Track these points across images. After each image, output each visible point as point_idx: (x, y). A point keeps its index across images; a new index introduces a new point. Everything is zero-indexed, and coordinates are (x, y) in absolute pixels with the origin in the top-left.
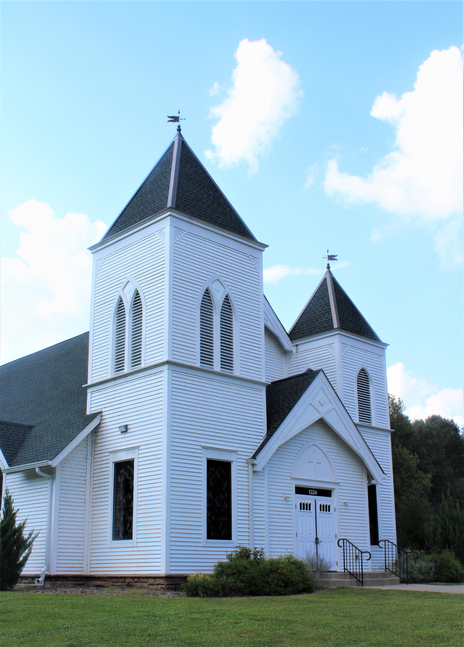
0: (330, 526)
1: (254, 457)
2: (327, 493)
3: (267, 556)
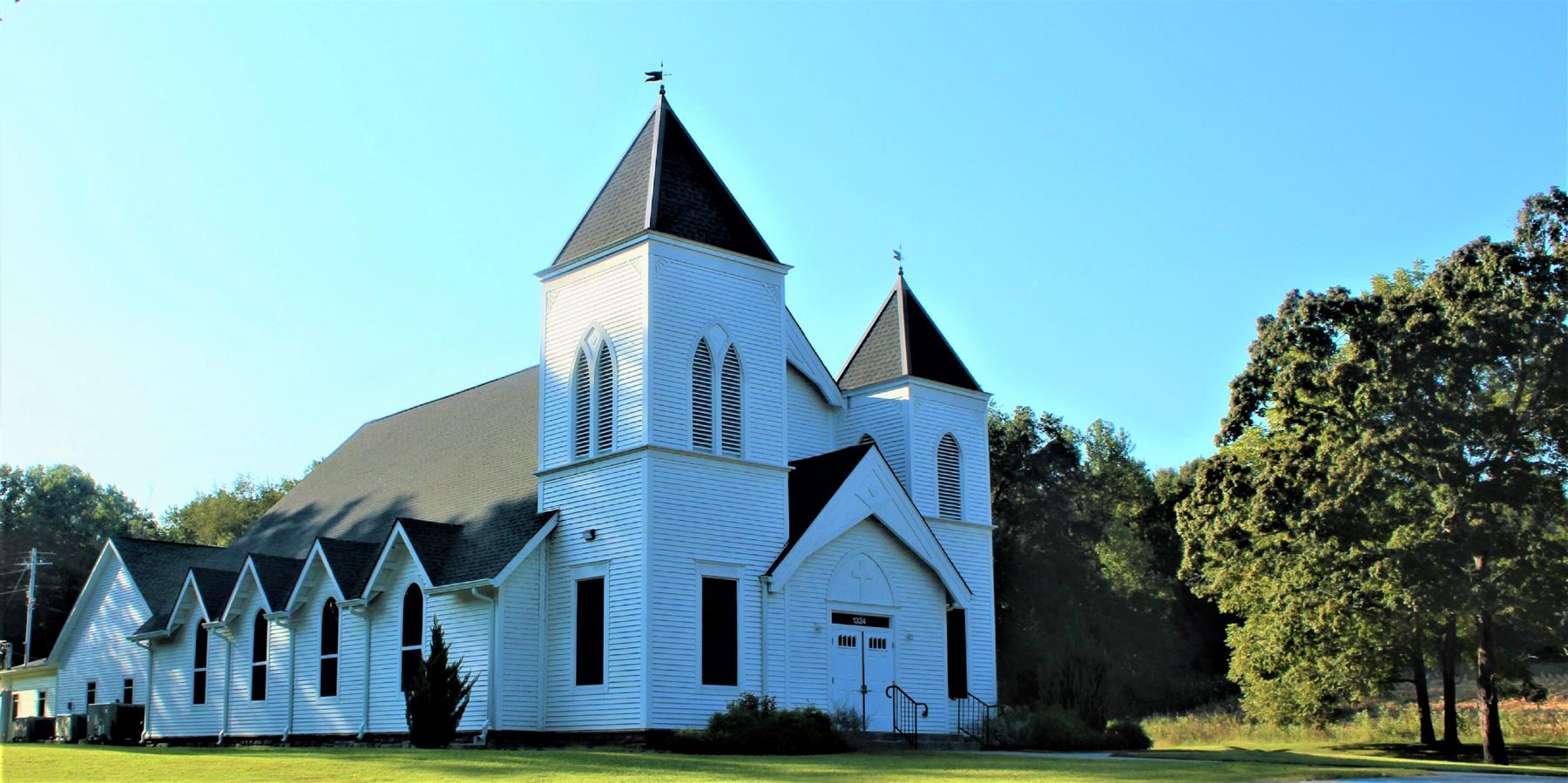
0: (881, 668)
1: (769, 573)
2: (883, 622)
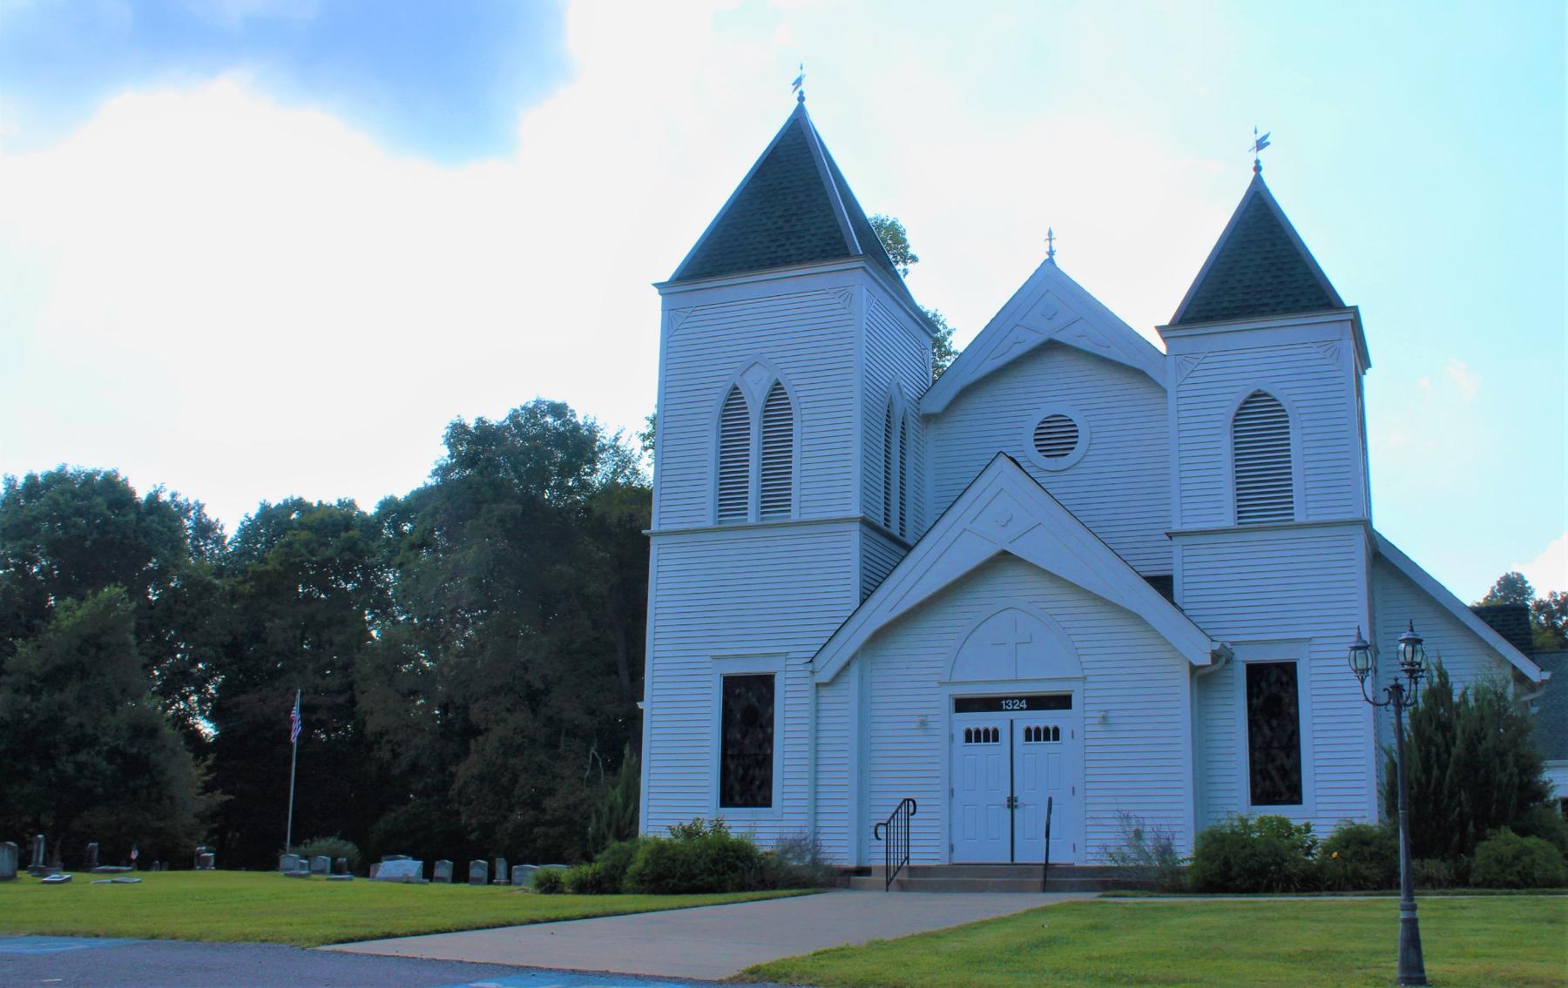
2: (1063, 702)
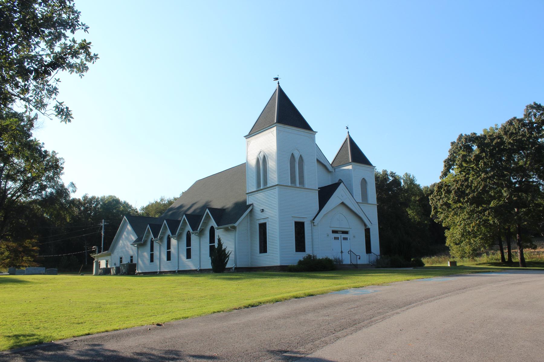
1: (314, 220)
2: (346, 233)
3: (318, 258)
